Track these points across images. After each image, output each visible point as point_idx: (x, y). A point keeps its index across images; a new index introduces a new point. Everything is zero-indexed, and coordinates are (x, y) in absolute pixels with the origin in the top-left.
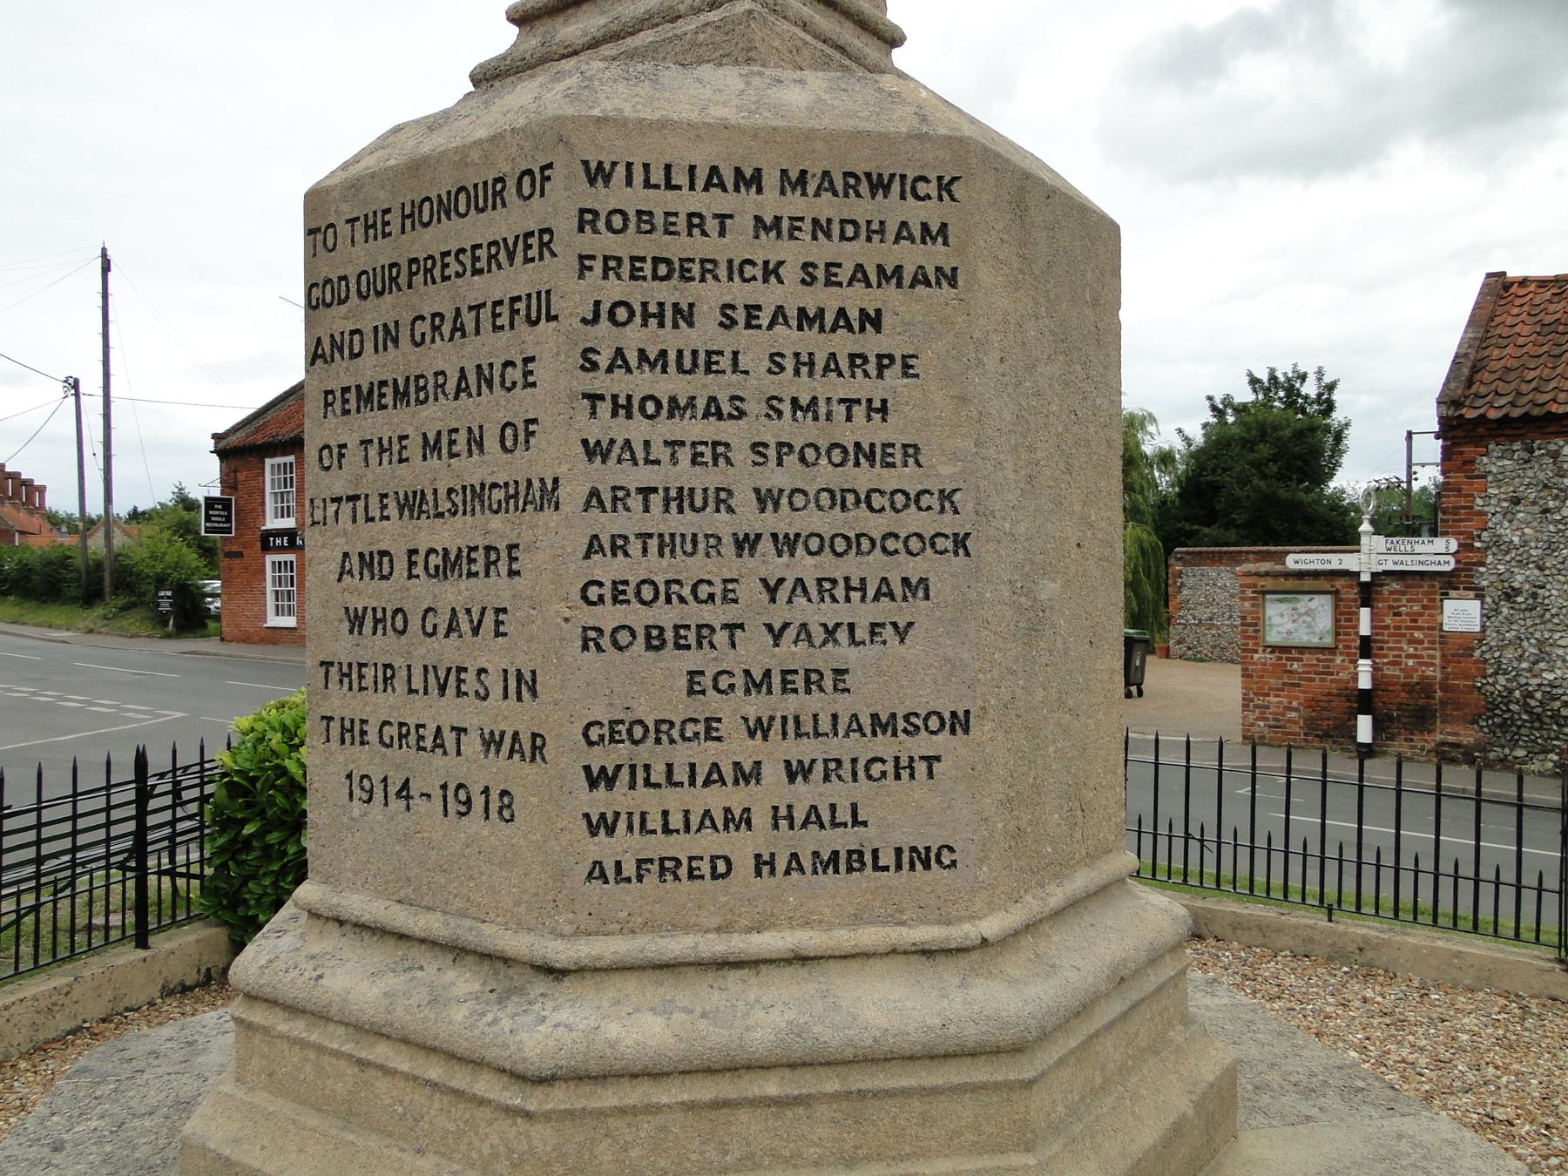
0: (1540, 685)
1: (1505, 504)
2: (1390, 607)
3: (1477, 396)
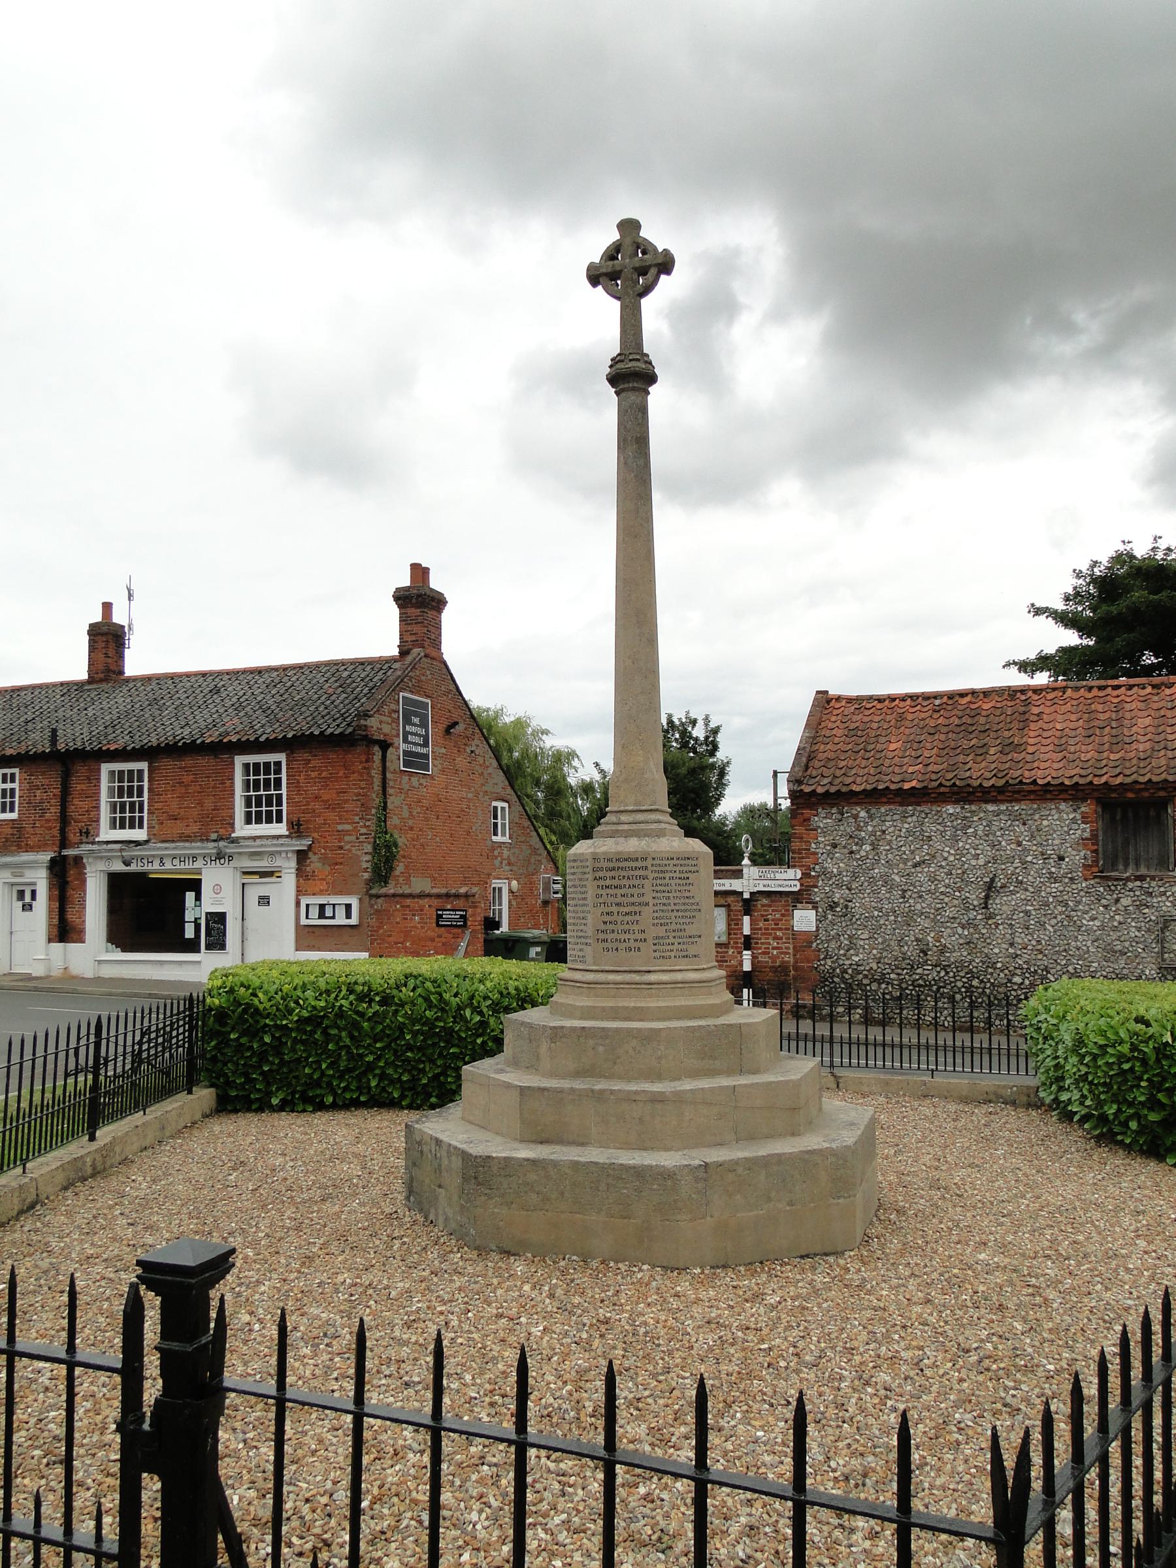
0: (851, 965)
1: (829, 848)
2: (762, 915)
3: (811, 777)
